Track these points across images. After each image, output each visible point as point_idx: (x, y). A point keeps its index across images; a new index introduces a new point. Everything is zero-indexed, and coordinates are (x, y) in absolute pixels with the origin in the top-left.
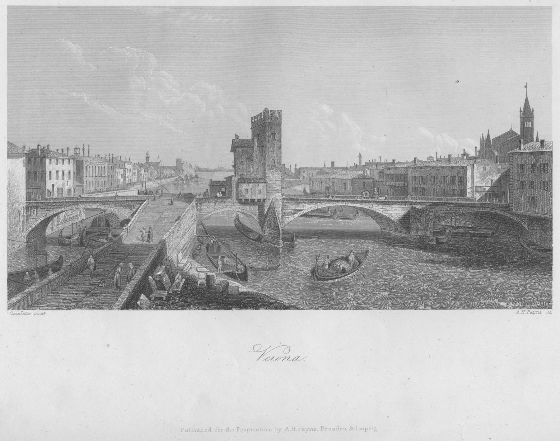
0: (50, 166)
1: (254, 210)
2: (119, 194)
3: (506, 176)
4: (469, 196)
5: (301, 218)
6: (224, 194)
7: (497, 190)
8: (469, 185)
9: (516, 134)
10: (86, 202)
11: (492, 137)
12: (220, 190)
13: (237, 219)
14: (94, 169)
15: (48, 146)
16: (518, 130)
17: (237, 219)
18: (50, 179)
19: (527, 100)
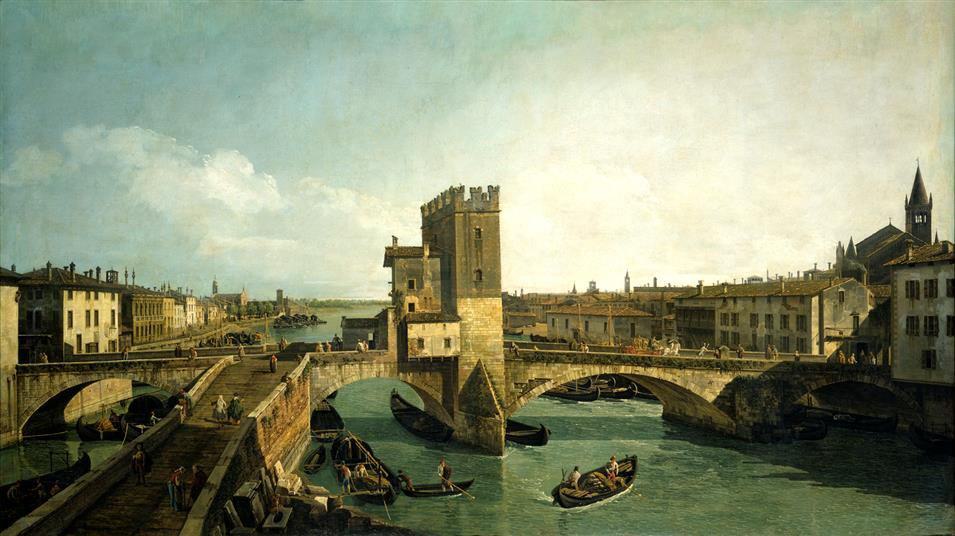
0: (76, 304)
1: (434, 384)
2: (880, 416)
3: (883, 312)
4: (815, 351)
5: (547, 402)
6: (372, 345)
7: (859, 343)
8: (815, 330)
9: (898, 231)
10: (92, 367)
11: (855, 243)
12: (362, 332)
13: (395, 396)
14: (139, 310)
15: (72, 265)
16: (900, 224)
17: (395, 396)
18: (71, 325)
19: (627, 278)
